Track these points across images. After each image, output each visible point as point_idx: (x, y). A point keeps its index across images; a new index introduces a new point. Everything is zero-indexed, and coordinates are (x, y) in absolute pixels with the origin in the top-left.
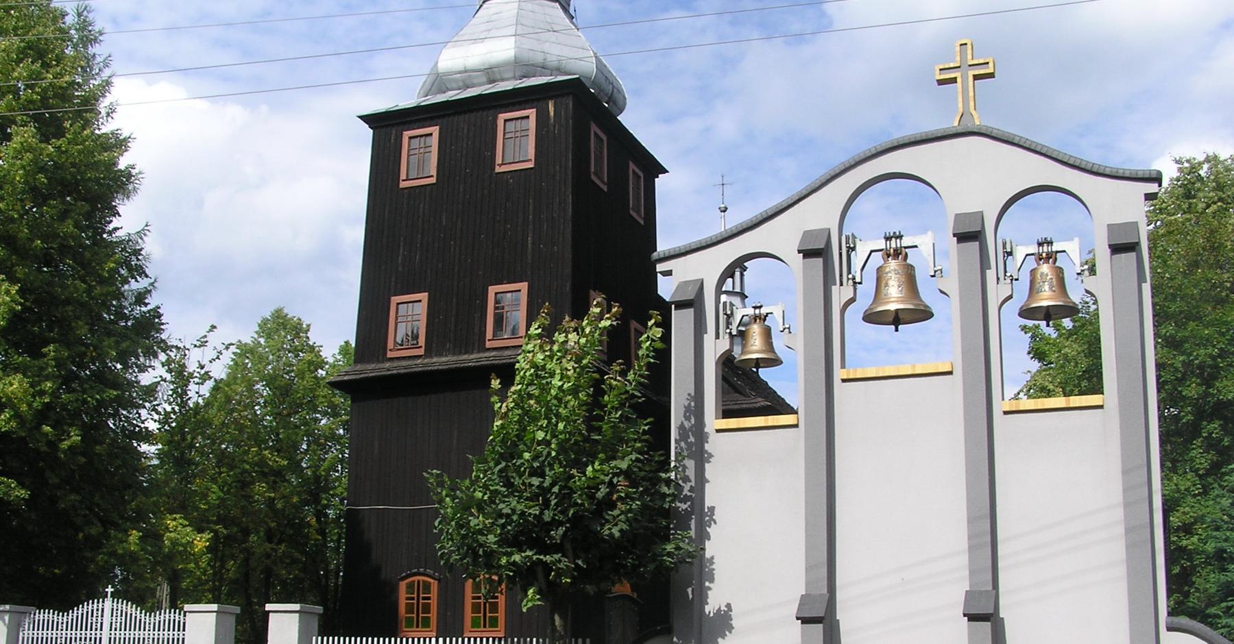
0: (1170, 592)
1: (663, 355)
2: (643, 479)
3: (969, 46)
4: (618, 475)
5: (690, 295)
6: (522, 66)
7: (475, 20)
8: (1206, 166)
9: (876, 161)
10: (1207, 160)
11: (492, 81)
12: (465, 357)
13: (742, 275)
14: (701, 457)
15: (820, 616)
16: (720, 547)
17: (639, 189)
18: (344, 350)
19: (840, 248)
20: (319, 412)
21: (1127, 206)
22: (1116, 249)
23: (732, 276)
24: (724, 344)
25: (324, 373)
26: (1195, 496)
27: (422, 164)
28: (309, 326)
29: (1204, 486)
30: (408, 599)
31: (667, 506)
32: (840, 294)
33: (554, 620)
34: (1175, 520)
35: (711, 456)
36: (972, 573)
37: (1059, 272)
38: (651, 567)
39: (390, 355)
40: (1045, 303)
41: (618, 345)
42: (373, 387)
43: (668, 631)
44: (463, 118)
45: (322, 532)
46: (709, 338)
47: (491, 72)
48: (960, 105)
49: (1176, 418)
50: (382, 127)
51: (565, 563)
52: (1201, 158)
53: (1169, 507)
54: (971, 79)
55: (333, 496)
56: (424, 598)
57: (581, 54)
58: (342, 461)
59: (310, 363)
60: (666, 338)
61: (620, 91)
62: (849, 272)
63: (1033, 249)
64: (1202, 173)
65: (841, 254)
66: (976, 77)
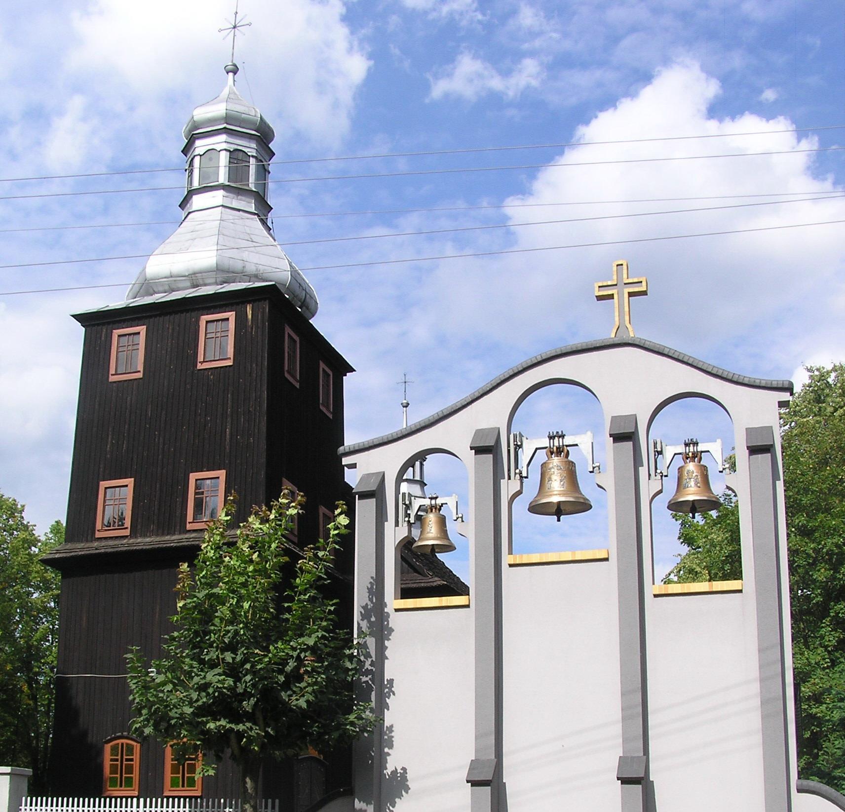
0: (800, 755)
1: (347, 540)
2: (328, 654)
3: (625, 267)
4: (305, 650)
5: (372, 487)
6: (223, 272)
7: (180, 230)
8: (833, 375)
9: (539, 368)
10: (834, 369)
11: (195, 286)
12: (167, 538)
13: (422, 465)
14: (381, 629)
15: (489, 780)
16: (396, 715)
17: (328, 386)
18: (56, 529)
19: (509, 446)
20: (32, 586)
21: (761, 412)
22: (753, 450)
23: (413, 467)
24: (403, 532)
25: (37, 550)
26: (824, 669)
27: (130, 360)
28: (23, 506)
29: (832, 661)
30: (112, 760)
31: (349, 679)
32: (508, 487)
33: (245, 783)
34: (805, 690)
35: (391, 630)
36: (625, 741)
37: (704, 471)
38: (335, 735)
39: (98, 535)
40: (691, 498)
41: (307, 530)
42: (81, 566)
43: (350, 793)
44: (170, 317)
45: (34, 698)
46: (389, 525)
47: (195, 279)
48: (617, 319)
49: (808, 598)
50: (94, 325)
51: (256, 731)
52: (829, 367)
53: (800, 678)
54: (626, 295)
55: (44, 664)
56: (127, 760)
57: (276, 263)
58: (52, 632)
59: (25, 541)
60: (351, 526)
61: (312, 297)
62: (516, 467)
63: (681, 449)
64: (830, 380)
65: (509, 451)
66: (631, 294)
